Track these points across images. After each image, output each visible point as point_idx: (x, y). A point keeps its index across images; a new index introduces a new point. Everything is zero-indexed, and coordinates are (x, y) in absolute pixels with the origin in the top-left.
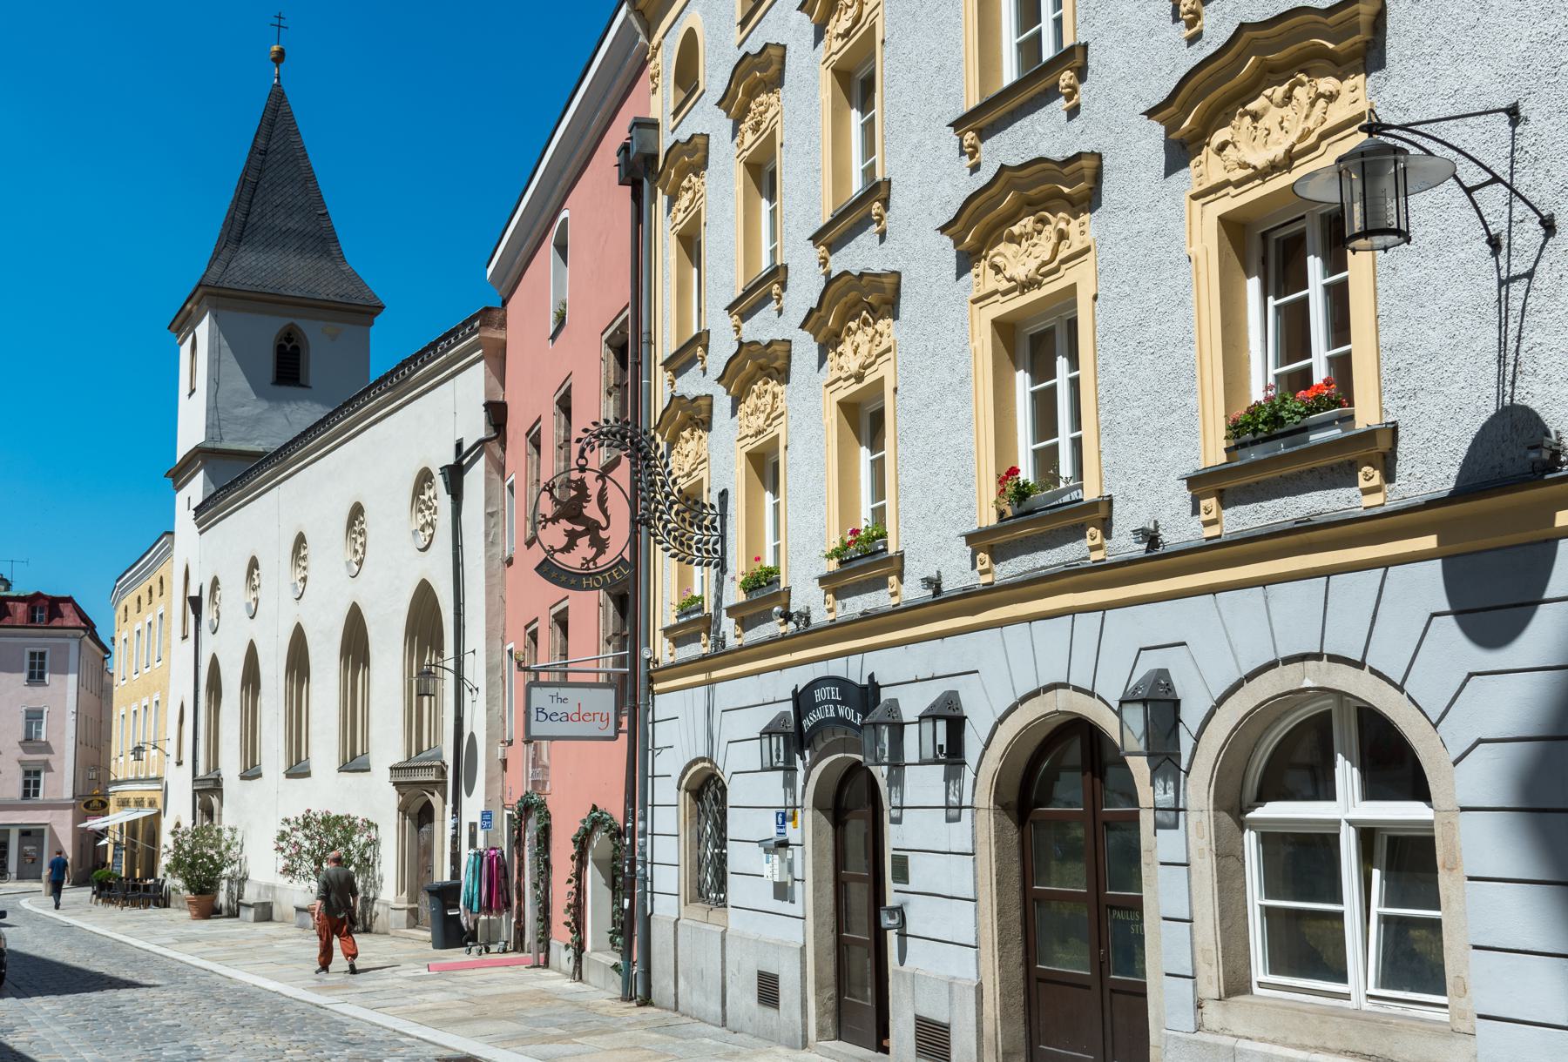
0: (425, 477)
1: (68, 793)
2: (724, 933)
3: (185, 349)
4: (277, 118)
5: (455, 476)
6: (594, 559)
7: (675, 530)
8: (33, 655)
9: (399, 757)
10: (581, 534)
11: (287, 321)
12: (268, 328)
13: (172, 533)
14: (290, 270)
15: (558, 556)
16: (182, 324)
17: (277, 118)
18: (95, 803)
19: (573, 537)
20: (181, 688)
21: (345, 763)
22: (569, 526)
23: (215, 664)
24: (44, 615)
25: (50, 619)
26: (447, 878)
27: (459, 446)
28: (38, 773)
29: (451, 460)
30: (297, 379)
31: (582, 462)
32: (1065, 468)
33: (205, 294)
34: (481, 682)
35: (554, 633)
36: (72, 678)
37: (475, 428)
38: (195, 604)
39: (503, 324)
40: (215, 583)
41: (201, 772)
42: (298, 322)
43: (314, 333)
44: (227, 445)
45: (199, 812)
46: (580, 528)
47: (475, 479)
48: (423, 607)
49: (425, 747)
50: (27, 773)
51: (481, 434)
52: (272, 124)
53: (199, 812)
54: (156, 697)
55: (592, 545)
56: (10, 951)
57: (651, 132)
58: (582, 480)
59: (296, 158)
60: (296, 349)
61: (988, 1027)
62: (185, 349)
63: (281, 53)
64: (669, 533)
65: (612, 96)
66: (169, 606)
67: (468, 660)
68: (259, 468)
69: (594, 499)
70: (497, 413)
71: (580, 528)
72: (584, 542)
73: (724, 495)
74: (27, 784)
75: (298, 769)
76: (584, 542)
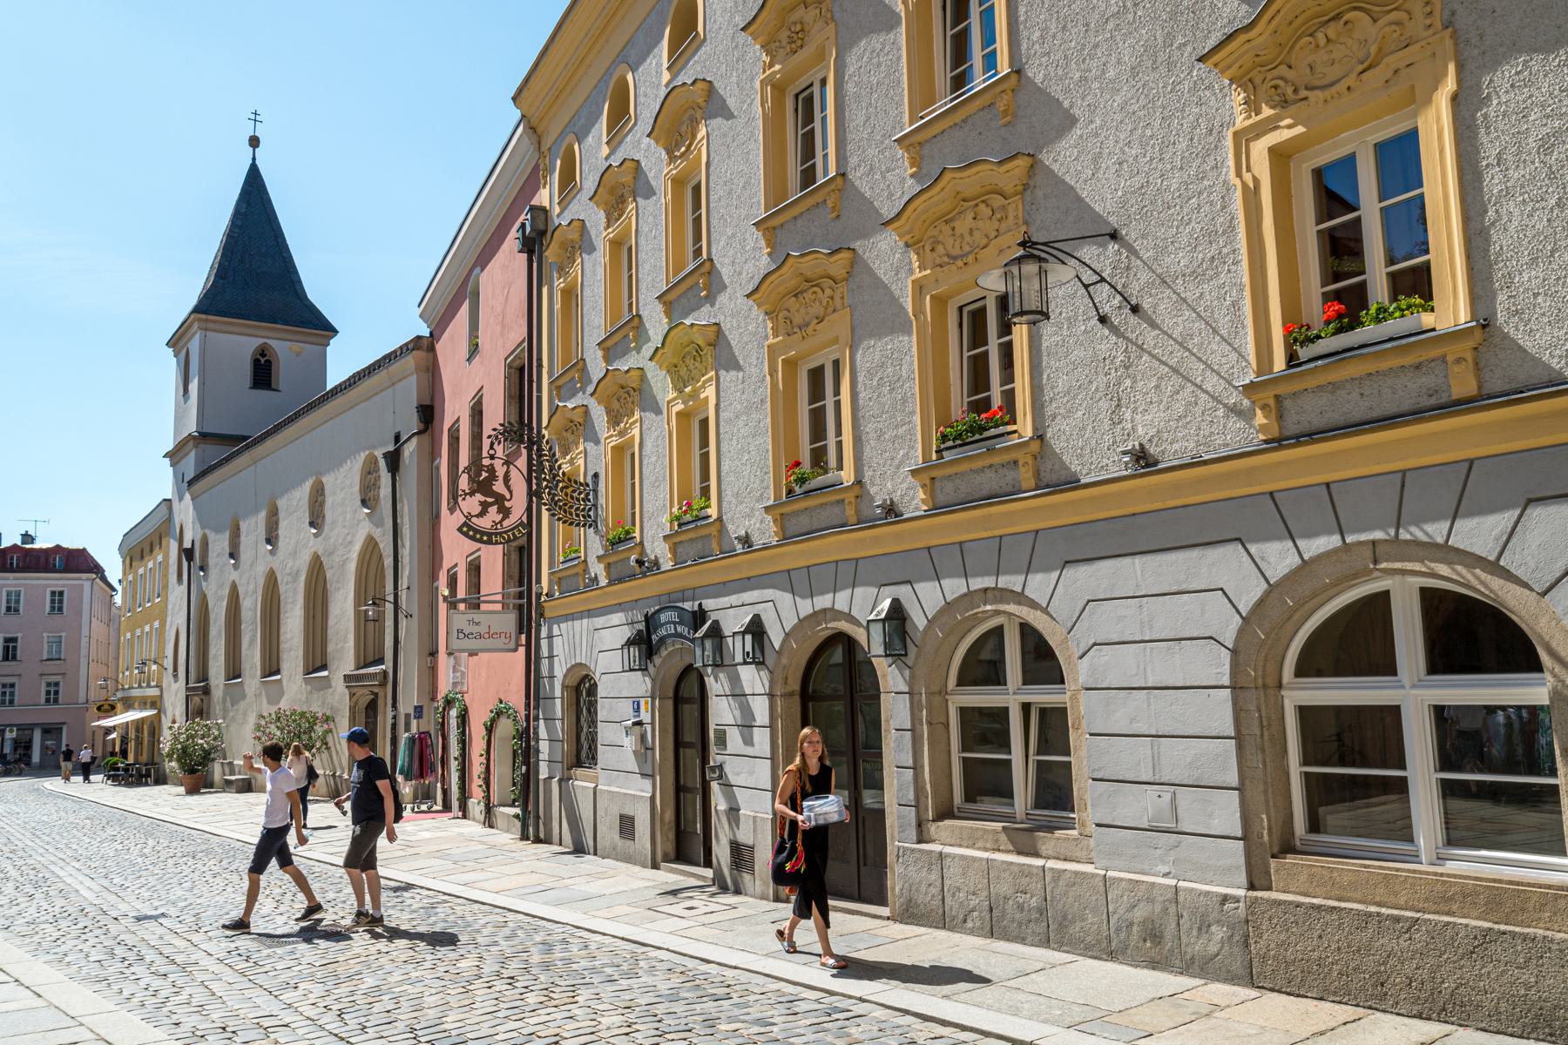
5: (394, 460)
10: (491, 504)
11: (258, 342)
19: (485, 507)
22: (483, 498)
27: (397, 438)
46: (490, 500)
55: (499, 511)
60: (268, 362)
69: (501, 479)
71: (490, 500)
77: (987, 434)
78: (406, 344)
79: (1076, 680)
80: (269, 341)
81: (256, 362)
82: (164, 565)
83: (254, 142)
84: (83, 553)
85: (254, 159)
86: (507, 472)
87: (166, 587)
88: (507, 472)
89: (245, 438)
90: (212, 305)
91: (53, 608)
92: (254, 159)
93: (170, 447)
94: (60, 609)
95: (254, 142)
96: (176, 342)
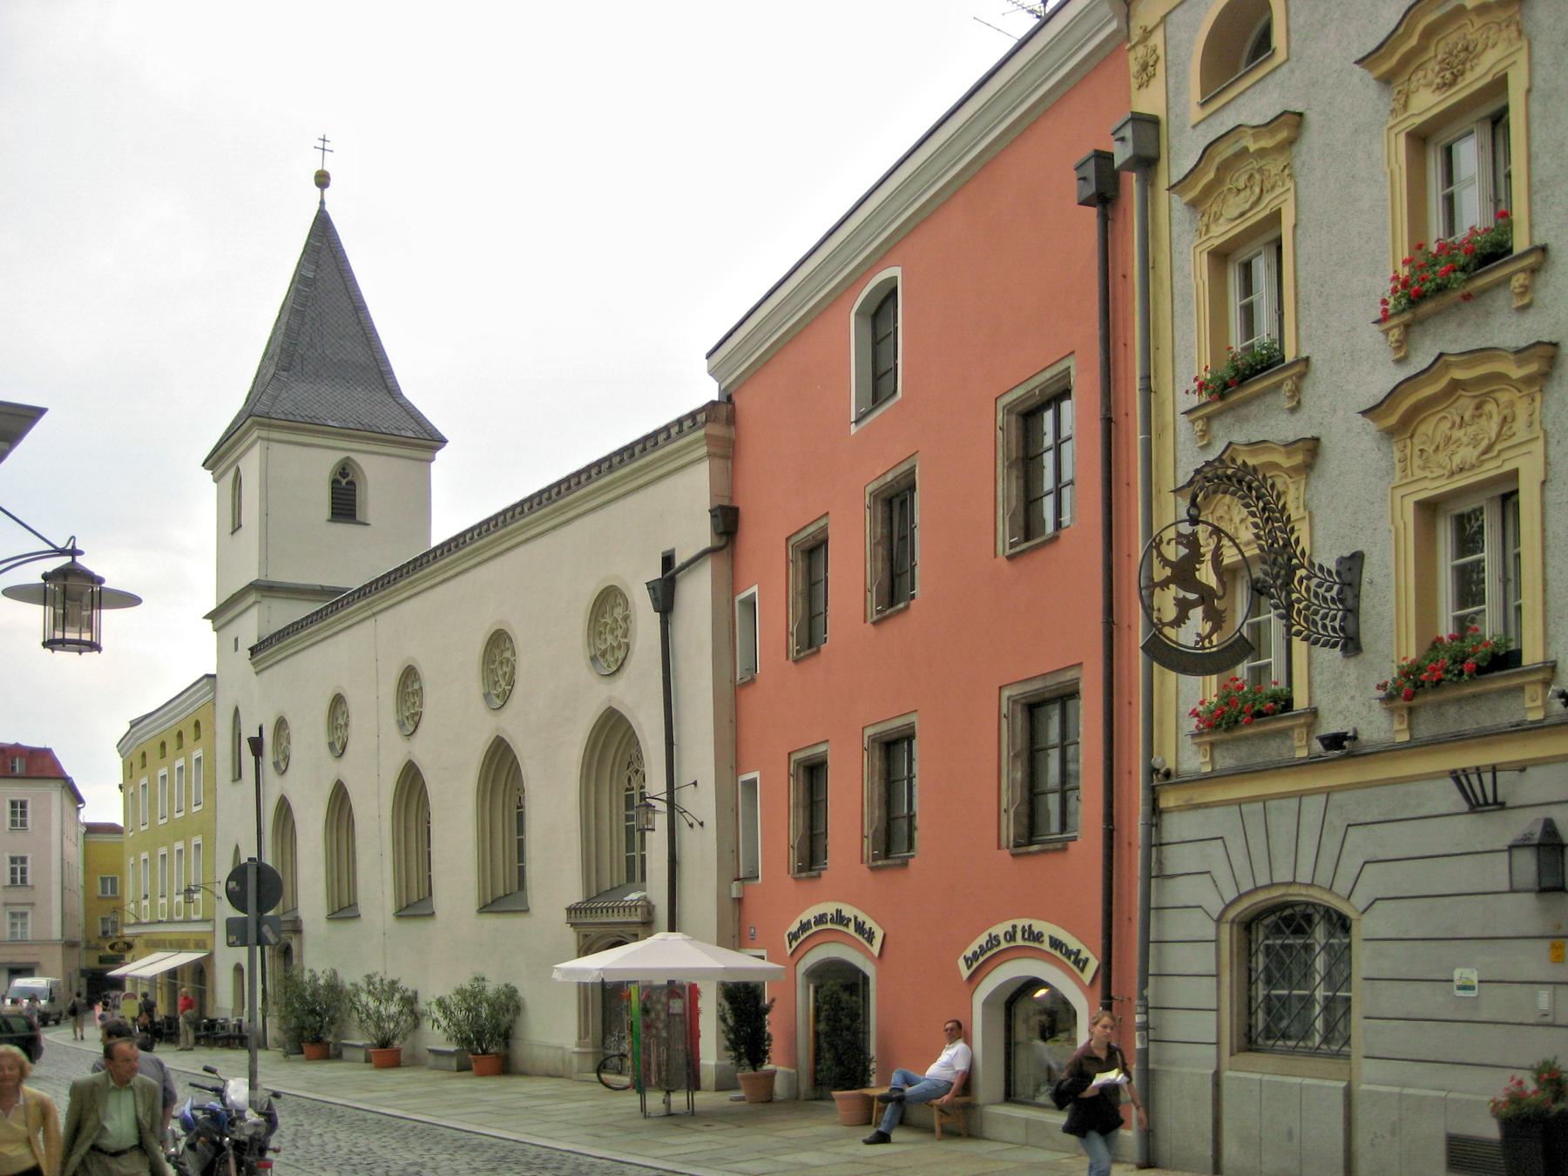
0: (608, 600)
1: (56, 934)
2: (1348, 1093)
5: (665, 595)
6: (1209, 636)
8: (13, 804)
9: (575, 895)
10: (1193, 604)
11: (341, 455)
12: (313, 466)
15: (1168, 631)
18: (121, 945)
19: (1184, 607)
22: (1181, 594)
23: (284, 807)
27: (668, 560)
30: (354, 516)
31: (1193, 512)
33: (254, 423)
37: (696, 534)
38: (257, 745)
40: (281, 724)
42: (355, 457)
43: (378, 472)
46: (1192, 596)
47: (697, 592)
48: (612, 734)
54: (198, 840)
55: (1206, 617)
58: (1194, 534)
60: (351, 483)
65: (1065, 88)
68: (336, 607)
69: (1208, 557)
70: (727, 521)
71: (1192, 596)
72: (1197, 613)
75: (415, 904)
76: (1197, 613)
77: (656, 784)
78: (693, 415)
79: (884, 1081)
80: (354, 456)
81: (335, 483)
82: (206, 764)
83: (322, 180)
84: (46, 754)
85: (322, 203)
86: (1218, 548)
87: (211, 790)
88: (1218, 548)
89: (341, 591)
90: (261, 415)
91: (14, 823)
92: (322, 203)
93: (214, 607)
94: (23, 824)
95: (322, 180)
96: (213, 461)
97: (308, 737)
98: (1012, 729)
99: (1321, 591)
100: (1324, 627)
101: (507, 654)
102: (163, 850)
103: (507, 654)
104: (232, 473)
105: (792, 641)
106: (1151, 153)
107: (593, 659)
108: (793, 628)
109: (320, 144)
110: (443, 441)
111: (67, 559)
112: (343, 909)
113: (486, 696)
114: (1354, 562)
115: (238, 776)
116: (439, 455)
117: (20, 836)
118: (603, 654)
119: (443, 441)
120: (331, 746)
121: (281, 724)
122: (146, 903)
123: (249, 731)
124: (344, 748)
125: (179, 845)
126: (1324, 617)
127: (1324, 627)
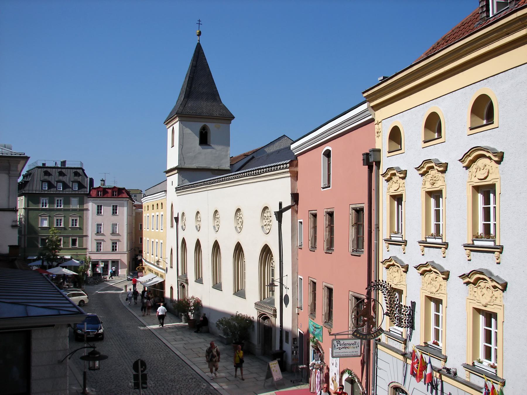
3: (170, 131)
4: (199, 55)
5: (279, 215)
7: (398, 316)
9: (258, 300)
11: (202, 124)
13: (166, 191)
14: (205, 106)
16: (169, 121)
17: (199, 55)
20: (171, 243)
21: (235, 292)
23: (184, 241)
24: (117, 193)
25: (118, 195)
26: (278, 349)
27: (280, 204)
28: (116, 243)
29: (278, 210)
32: (492, 232)
34: (290, 286)
35: (324, 291)
36: (125, 209)
37: (287, 202)
38: (177, 219)
39: (297, 166)
40: (183, 214)
41: (180, 274)
42: (207, 124)
43: (212, 127)
44: (187, 166)
45: (179, 287)
47: (287, 216)
48: (266, 251)
49: (266, 297)
50: (113, 243)
51: (289, 204)
52: (198, 57)
53: (179, 287)
54: (161, 241)
56: (83, 213)
57: (378, 153)
59: (206, 67)
60: (206, 133)
61: (362, 230)
62: (170, 131)
63: (200, 33)
64: (395, 318)
66: (165, 212)
67: (284, 279)
70: (295, 197)
73: (413, 304)
74: (113, 247)
95: (200, 34)
97: (190, 221)
98: (352, 304)
99: (404, 313)
100: (405, 323)
101: (241, 216)
102: (153, 240)
103: (241, 216)
104: (172, 127)
105: (310, 242)
106: (379, 160)
107: (262, 227)
108: (310, 239)
109: (200, 23)
110: (233, 118)
111: (92, 349)
112: (199, 280)
113: (236, 227)
114: (413, 304)
115: (172, 227)
116: (232, 121)
117: (115, 217)
118: (265, 225)
119: (233, 118)
120: (196, 226)
121: (183, 214)
122: (148, 254)
123: (175, 215)
124: (200, 228)
125: (157, 240)
126: (405, 320)
127: (405, 323)
